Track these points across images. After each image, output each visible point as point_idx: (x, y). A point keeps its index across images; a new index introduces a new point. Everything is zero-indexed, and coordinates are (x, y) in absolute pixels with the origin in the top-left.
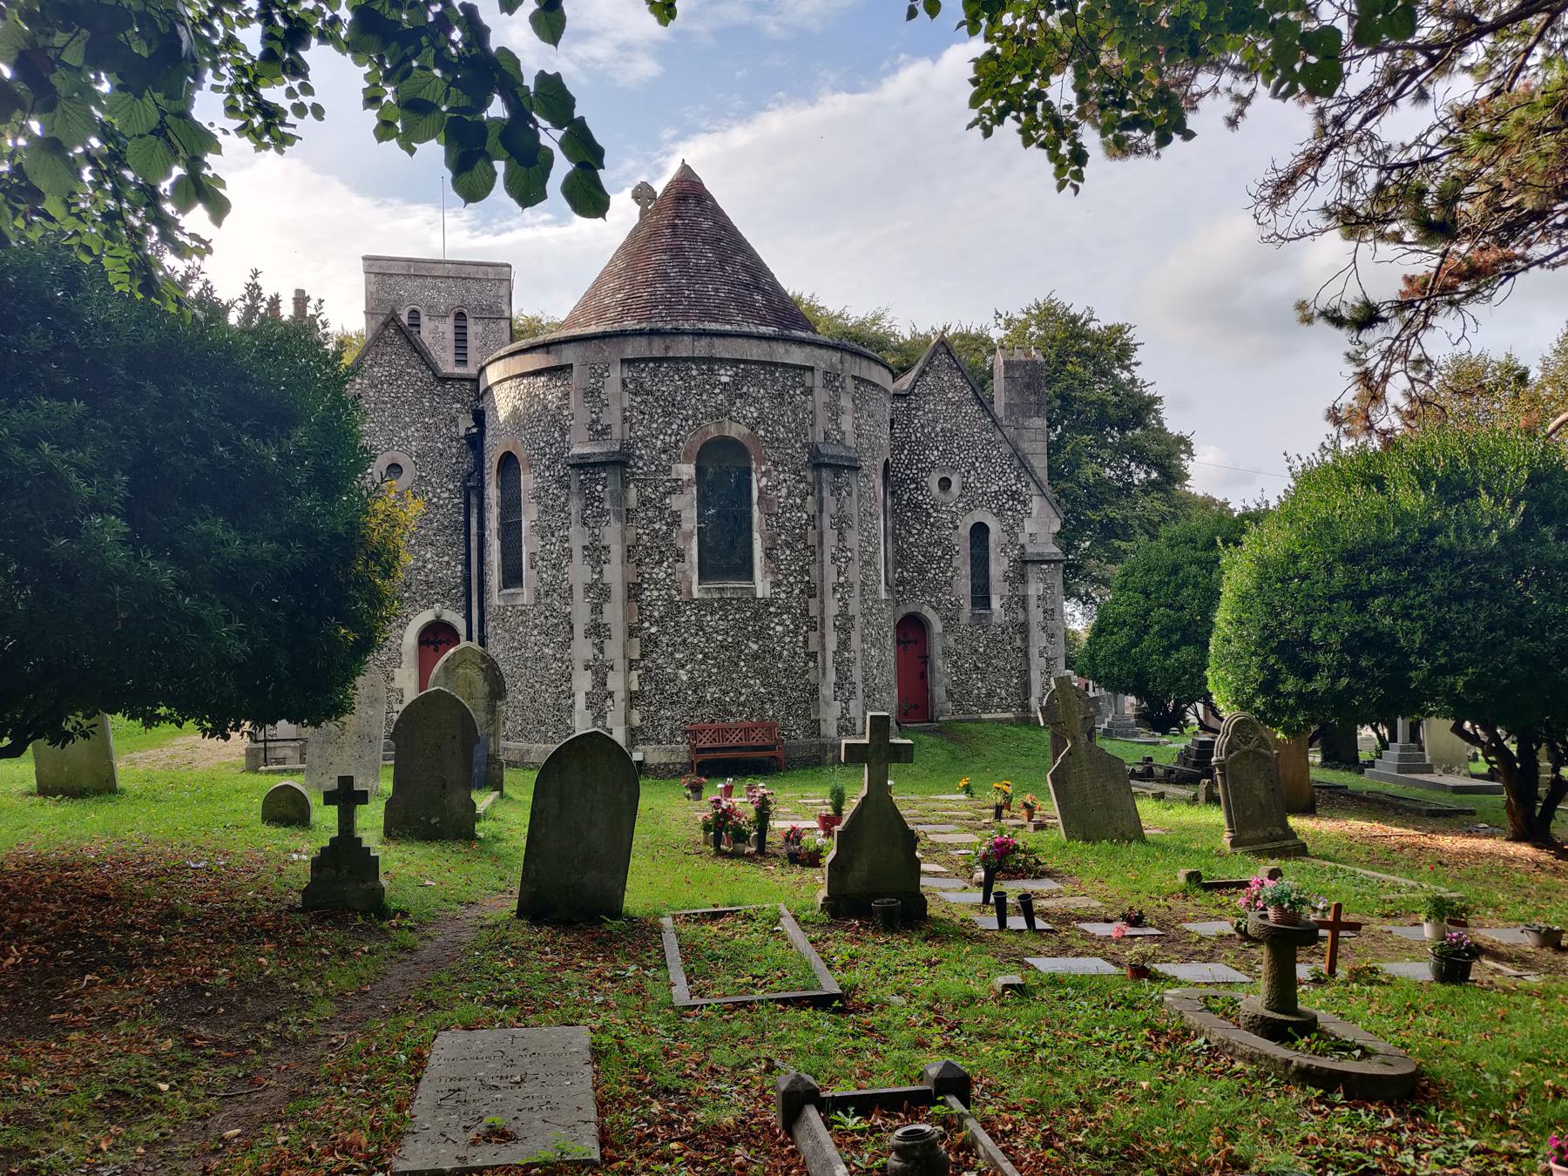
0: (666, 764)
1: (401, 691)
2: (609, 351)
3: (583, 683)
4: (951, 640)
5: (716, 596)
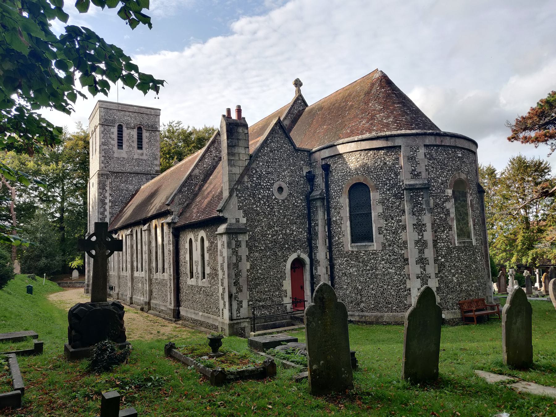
0: (453, 319)
1: (286, 291)
2: (419, 141)
5: (463, 245)
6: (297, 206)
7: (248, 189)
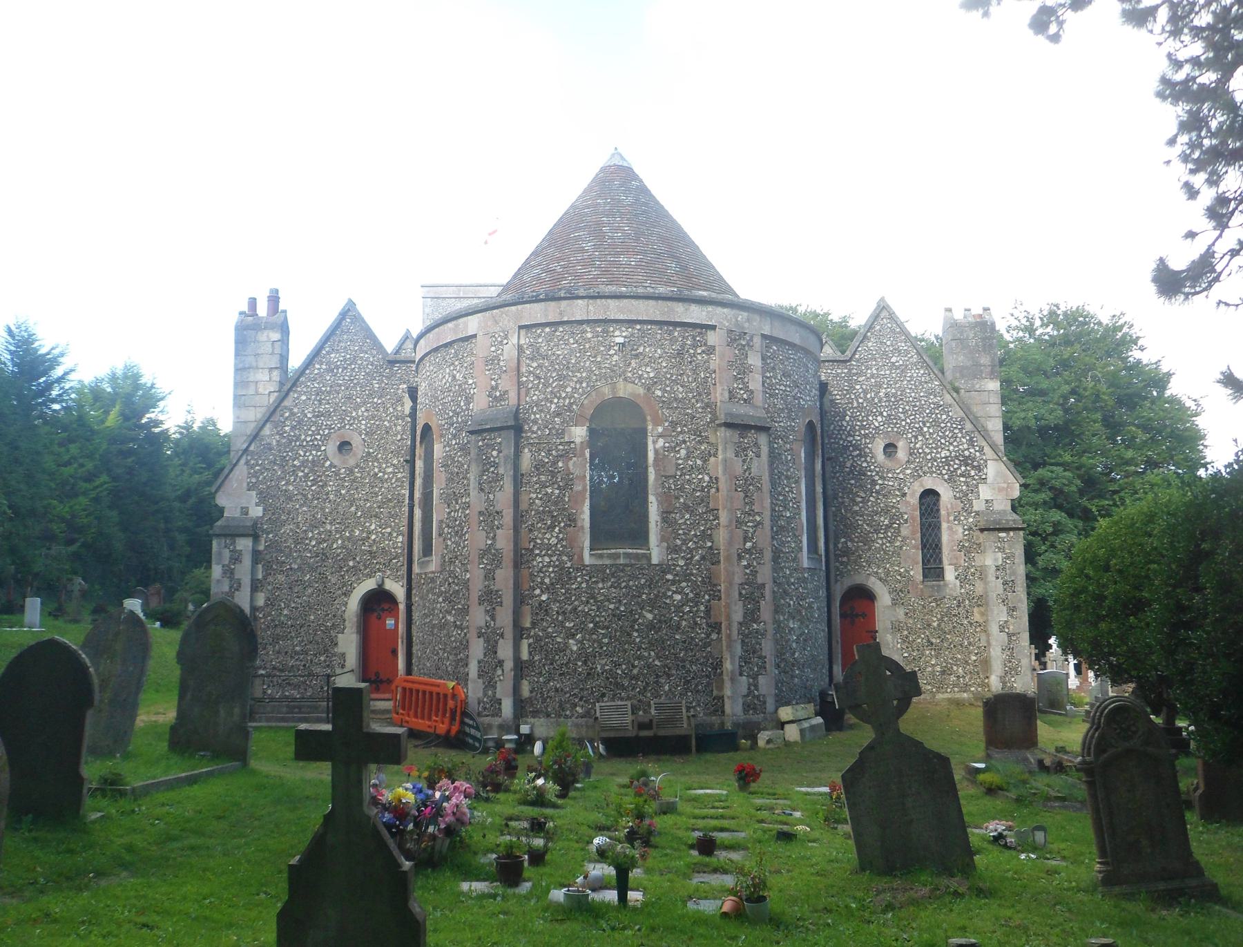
1: (343, 655)
3: (477, 649)
4: (900, 612)
6: (382, 480)
7: (271, 449)
